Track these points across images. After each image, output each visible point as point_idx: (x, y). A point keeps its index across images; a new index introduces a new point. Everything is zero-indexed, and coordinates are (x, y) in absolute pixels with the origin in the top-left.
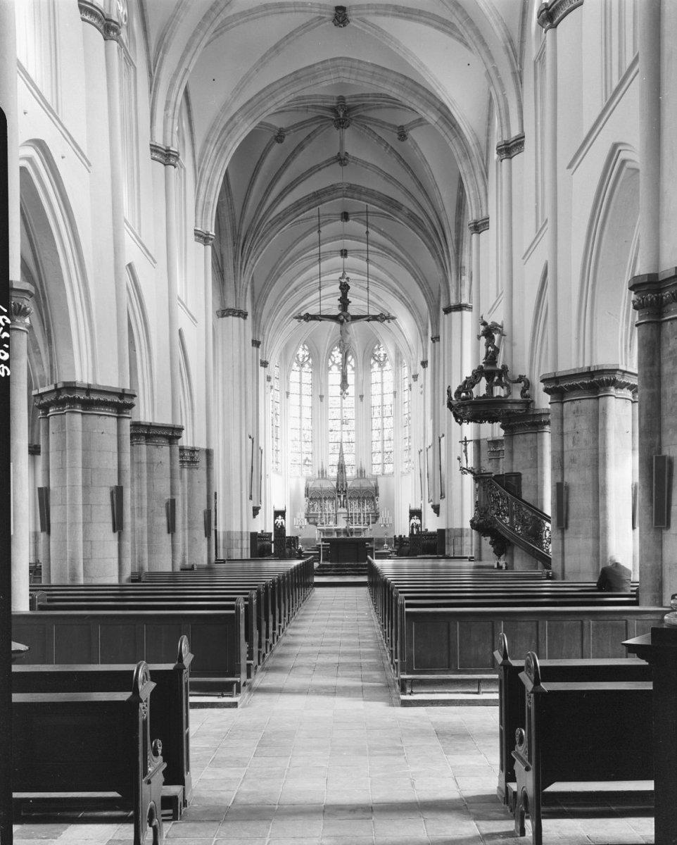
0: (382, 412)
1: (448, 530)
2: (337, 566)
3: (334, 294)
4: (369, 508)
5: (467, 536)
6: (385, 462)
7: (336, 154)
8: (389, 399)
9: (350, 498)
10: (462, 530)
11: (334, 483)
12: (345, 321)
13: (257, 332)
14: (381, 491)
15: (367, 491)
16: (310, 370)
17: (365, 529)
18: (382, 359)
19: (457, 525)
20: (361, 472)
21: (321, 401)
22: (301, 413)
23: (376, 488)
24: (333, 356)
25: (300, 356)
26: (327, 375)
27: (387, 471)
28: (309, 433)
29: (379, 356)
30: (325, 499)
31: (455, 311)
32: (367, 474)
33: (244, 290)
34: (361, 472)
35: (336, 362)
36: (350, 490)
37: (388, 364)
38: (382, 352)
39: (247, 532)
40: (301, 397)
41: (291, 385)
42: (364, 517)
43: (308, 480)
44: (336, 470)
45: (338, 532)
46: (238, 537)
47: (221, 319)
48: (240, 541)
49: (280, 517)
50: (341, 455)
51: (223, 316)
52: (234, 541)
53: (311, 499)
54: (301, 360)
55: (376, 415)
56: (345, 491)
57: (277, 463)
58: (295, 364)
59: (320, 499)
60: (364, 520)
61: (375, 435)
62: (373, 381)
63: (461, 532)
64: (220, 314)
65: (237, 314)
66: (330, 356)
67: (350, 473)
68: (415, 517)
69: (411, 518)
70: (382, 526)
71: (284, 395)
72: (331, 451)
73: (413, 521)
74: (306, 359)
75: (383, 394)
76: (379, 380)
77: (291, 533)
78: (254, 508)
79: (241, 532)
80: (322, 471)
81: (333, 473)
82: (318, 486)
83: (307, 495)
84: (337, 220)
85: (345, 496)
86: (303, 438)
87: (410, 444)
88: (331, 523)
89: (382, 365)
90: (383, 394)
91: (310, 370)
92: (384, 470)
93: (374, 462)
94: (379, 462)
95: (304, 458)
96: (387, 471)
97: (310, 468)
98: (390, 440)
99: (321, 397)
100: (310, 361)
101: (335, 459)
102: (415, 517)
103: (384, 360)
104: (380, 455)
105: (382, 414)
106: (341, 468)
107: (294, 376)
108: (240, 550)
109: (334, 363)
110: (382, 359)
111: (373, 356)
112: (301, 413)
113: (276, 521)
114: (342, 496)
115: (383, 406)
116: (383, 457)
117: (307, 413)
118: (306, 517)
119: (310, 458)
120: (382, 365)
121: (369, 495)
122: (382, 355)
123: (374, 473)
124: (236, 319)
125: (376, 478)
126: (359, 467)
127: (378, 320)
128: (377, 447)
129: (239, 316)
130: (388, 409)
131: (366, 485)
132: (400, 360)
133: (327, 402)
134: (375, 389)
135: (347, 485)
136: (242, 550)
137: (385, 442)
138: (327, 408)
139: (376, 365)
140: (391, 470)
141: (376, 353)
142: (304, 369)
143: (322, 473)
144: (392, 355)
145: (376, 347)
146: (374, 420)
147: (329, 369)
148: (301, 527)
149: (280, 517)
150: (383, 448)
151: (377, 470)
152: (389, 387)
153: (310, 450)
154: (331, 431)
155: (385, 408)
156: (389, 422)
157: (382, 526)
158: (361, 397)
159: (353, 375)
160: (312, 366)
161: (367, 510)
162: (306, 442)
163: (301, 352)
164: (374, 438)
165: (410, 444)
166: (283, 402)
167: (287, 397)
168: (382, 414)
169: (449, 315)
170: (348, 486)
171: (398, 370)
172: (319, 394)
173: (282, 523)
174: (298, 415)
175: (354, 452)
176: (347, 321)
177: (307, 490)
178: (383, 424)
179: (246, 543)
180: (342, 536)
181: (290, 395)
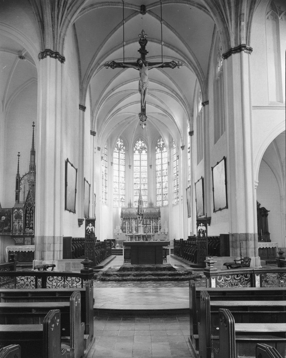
0: (162, 173)
1: (233, 235)
2: (137, 269)
3: (137, 102)
4: (155, 224)
5: (251, 240)
6: (164, 199)
7: (139, 52)
8: (165, 167)
9: (145, 218)
10: (247, 235)
11: (137, 211)
12: (144, 65)
13: (83, 100)
14: (162, 215)
15: (154, 214)
16: (124, 152)
17: (153, 235)
18: (161, 147)
19: (241, 230)
20: (151, 204)
21: (130, 168)
22: (119, 174)
23: (159, 213)
24: (136, 145)
25: (119, 145)
26: (133, 155)
27: (164, 204)
28: (123, 185)
29: (160, 145)
30: (132, 219)
31: (235, 53)
32: (154, 205)
33: (61, 39)
34: (151, 204)
35: (138, 149)
36: (145, 214)
37: (165, 148)
38: (162, 143)
39: (60, 237)
40: (119, 166)
41: (114, 160)
42: (153, 229)
43: (122, 209)
44: (137, 204)
45: (139, 237)
46: (51, 241)
47: (41, 60)
48: (52, 245)
49: (91, 225)
50: (140, 196)
51: (42, 58)
52: (47, 245)
53: (124, 219)
54: (119, 147)
55: (159, 175)
56: (143, 215)
57: (106, 199)
58: (116, 149)
59: (129, 219)
60: (153, 230)
61: (158, 185)
62: (157, 157)
63: (246, 237)
64: (40, 57)
65: (54, 55)
66: (134, 145)
67: (145, 205)
68: (202, 224)
69: (198, 225)
70: (163, 233)
71: (110, 164)
72: (135, 194)
73: (199, 228)
74: (122, 147)
75: (162, 164)
76: (160, 157)
77: (40, 235)
78: (79, 220)
79: (54, 237)
80: (151, 204)
81: (136, 205)
82: (128, 212)
83: (122, 217)
84: (137, 93)
85: (142, 217)
86: (120, 187)
87: (178, 189)
88: (134, 232)
89: (161, 149)
90: (162, 164)
91: (124, 152)
92: (163, 204)
93: (158, 200)
94: (160, 199)
95: (121, 197)
96: (164, 204)
97: (124, 203)
98: (166, 188)
99: (130, 166)
100: (124, 148)
101: (137, 198)
102: (202, 224)
103: (163, 147)
104: (161, 196)
105: (162, 175)
106: (140, 202)
107: (116, 155)
108: (52, 252)
109: (136, 149)
110: (161, 147)
111: (157, 145)
112: (119, 174)
113: (88, 227)
114: (141, 217)
115: (162, 170)
116: (162, 197)
117: (122, 174)
118: (121, 229)
119: (124, 198)
120: (161, 149)
121: (155, 216)
122: (161, 145)
123: (158, 205)
124: (53, 60)
125: (159, 208)
126: (150, 201)
127: (170, 67)
128: (159, 192)
129: (56, 57)
130: (165, 172)
131: (153, 211)
132: (171, 145)
133: (133, 169)
134: (158, 162)
135: (143, 211)
136: (54, 253)
137: (163, 189)
138: (133, 172)
139: (158, 150)
140: (167, 204)
141: (159, 144)
142: (120, 152)
143: (130, 205)
144: (167, 142)
145: (159, 140)
146: (157, 178)
147: (134, 152)
148: (118, 234)
149: (91, 225)
150: (162, 192)
151: (159, 204)
152: (165, 161)
153: (124, 193)
154: (135, 184)
155: (164, 172)
156: (165, 179)
157: (163, 233)
158: (151, 166)
159: (146, 156)
160: (124, 151)
161: (154, 225)
162: (122, 189)
163: (119, 143)
164: (158, 187)
165: (178, 189)
166: (109, 167)
167: (112, 165)
168: (162, 175)
169: (229, 58)
170: (144, 212)
171: (170, 151)
172: (129, 164)
173: (92, 229)
174: (118, 175)
175: (147, 194)
176: (146, 66)
177: (122, 214)
178: (162, 179)
179: (59, 247)
180: (141, 241)
181: (113, 165)
